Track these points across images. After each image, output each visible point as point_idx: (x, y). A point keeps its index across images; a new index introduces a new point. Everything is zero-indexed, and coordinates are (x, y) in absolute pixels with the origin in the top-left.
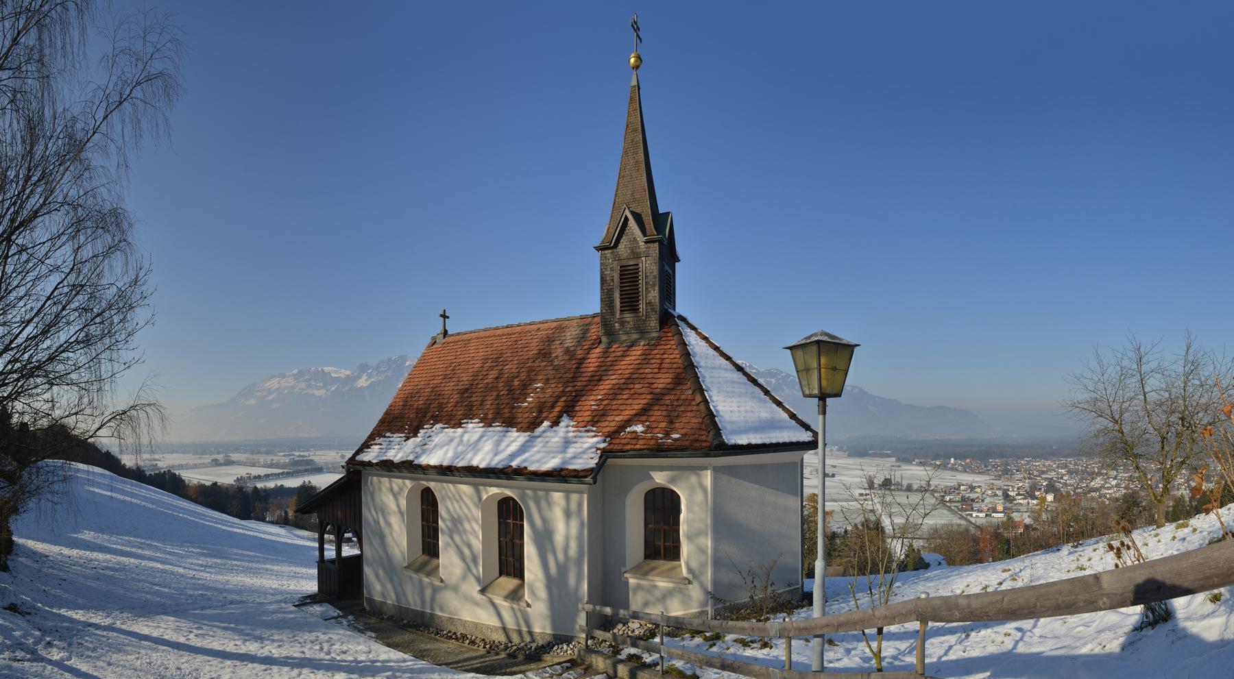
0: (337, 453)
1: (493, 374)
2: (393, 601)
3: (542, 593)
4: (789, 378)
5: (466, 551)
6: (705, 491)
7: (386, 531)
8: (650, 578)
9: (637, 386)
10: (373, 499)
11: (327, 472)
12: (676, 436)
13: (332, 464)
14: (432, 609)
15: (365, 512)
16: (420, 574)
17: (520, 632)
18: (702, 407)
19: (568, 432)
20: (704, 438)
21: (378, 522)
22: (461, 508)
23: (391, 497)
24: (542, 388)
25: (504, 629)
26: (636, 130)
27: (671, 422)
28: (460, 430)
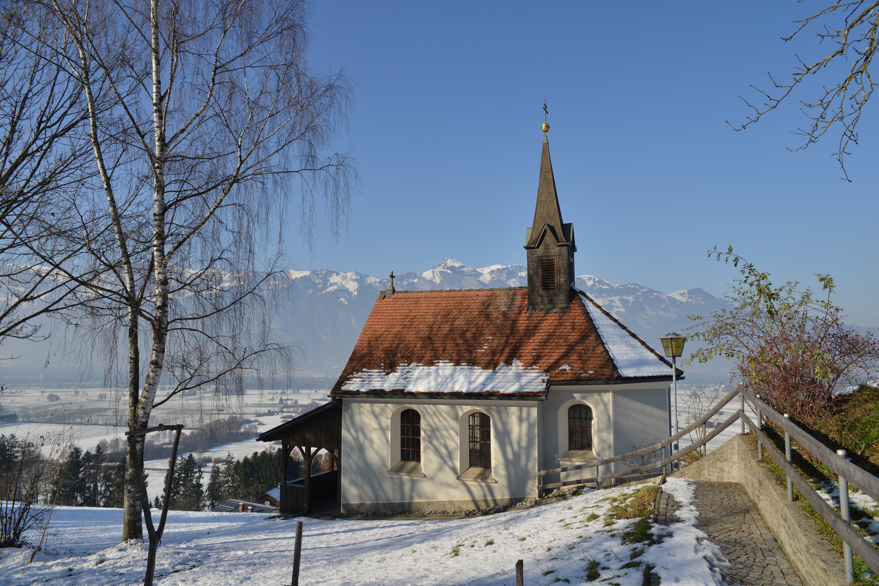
0: (43, 392)
1: (446, 327)
3: (502, 472)
4: (653, 294)
5: (443, 450)
6: (606, 405)
9: (560, 341)
11: (24, 422)
12: (591, 372)
13: (35, 409)
14: (412, 498)
15: (344, 433)
17: (486, 501)
22: (440, 421)
23: (373, 418)
26: (547, 172)
28: (433, 368)
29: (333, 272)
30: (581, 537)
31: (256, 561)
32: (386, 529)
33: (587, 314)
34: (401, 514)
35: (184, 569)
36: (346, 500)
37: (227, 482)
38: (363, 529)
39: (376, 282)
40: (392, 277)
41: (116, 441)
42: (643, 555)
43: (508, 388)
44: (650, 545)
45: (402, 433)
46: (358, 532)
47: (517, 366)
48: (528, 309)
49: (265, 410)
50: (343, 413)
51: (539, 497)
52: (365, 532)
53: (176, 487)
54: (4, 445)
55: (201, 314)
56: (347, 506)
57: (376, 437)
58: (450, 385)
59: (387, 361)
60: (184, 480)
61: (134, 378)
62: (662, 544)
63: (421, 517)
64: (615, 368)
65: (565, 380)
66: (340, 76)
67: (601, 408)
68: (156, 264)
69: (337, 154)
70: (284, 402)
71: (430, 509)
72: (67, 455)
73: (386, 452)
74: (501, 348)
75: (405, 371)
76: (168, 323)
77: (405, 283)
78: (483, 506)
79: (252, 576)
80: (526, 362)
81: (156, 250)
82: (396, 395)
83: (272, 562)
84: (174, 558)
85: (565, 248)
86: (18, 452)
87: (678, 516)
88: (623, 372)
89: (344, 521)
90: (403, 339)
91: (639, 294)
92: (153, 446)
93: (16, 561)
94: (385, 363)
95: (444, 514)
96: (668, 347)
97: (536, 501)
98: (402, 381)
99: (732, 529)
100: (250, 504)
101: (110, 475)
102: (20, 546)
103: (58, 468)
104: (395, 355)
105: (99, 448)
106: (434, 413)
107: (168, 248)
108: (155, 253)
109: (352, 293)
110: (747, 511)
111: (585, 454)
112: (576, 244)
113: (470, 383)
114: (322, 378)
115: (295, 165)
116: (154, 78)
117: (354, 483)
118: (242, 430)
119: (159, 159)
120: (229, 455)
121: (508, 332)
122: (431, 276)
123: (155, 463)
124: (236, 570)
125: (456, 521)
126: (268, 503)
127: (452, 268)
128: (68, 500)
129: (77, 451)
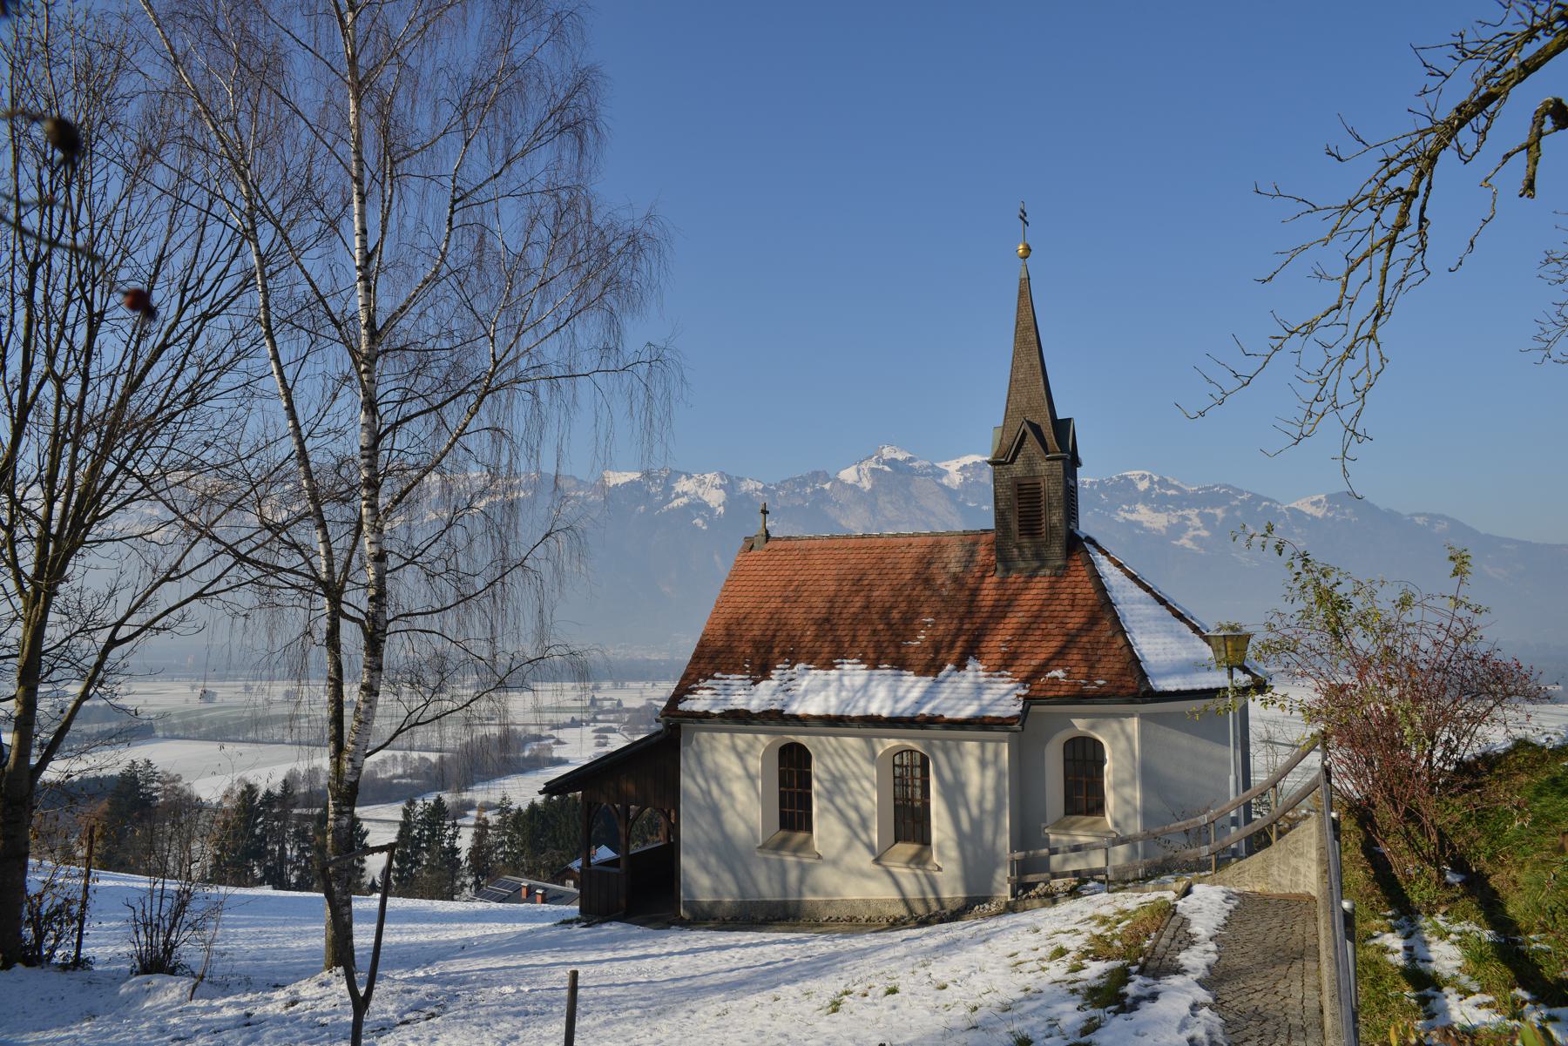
0: (193, 687)
1: (858, 602)
2: (732, 895)
3: (953, 852)
5: (853, 815)
6: (1129, 739)
7: (724, 803)
8: (1073, 832)
9: (1050, 626)
10: (700, 762)
11: (166, 738)
12: (1101, 682)
13: (182, 715)
14: (800, 893)
15: (685, 782)
16: (783, 853)
17: (925, 901)
18: (1125, 650)
19: (977, 677)
20: (1131, 684)
21: (709, 793)
22: (846, 765)
23: (733, 758)
24: (934, 625)
25: (906, 901)
27: (1092, 667)
28: (833, 672)
29: (681, 473)
30: (1026, 990)
31: (531, 1008)
32: (749, 950)
33: (1097, 577)
34: (779, 920)
35: (417, 1020)
36: (689, 893)
37: (502, 844)
38: (712, 949)
39: (756, 490)
40: (765, 512)
41: (313, 773)
42: (1099, 1031)
43: (959, 710)
44: (1116, 1013)
45: (782, 783)
46: (703, 954)
47: (975, 671)
48: (996, 570)
49: (565, 718)
50: (682, 749)
51: (1013, 896)
52: (715, 955)
53: (415, 854)
54: (135, 777)
55: (438, 606)
56: (693, 905)
57: (739, 789)
58: (862, 703)
59: (757, 662)
60: (428, 841)
61: (336, 711)
62: (1134, 1014)
63: (812, 926)
64: (1144, 676)
65: (1055, 696)
66: (649, 218)
67: (1122, 744)
68: (365, 527)
69: (649, 344)
70: (598, 703)
71: (833, 913)
72: (234, 796)
73: (756, 815)
74: (949, 638)
75: (786, 678)
76: (388, 622)
77: (809, 490)
78: (920, 910)
79: (521, 1032)
80: (992, 662)
81: (366, 506)
82: (771, 719)
83: (555, 1009)
84: (403, 1000)
85: (1060, 463)
86: (157, 789)
87: (1181, 962)
88: (1157, 683)
89: (683, 933)
90: (783, 621)
91: (1235, 503)
92: (375, 780)
93: (171, 995)
94: (751, 664)
95: (855, 922)
96: (1219, 650)
97: (1008, 903)
98: (781, 696)
99: (1259, 988)
100: (541, 886)
101: (306, 830)
102: (172, 972)
103: (220, 817)
104: (770, 650)
105: (286, 784)
106: (836, 751)
107: (383, 501)
108: (365, 511)
109: (714, 510)
110: (1302, 956)
111: (1095, 823)
112: (1081, 454)
113: (896, 701)
114: (665, 661)
115: (587, 362)
116: (357, 226)
117: (705, 867)
118: (527, 753)
119: (367, 357)
120: (504, 799)
121: (962, 609)
122: (856, 477)
123: (381, 810)
124: (497, 1023)
125: (868, 936)
126: (572, 882)
127: (892, 462)
128: (243, 879)
129: (251, 790)
